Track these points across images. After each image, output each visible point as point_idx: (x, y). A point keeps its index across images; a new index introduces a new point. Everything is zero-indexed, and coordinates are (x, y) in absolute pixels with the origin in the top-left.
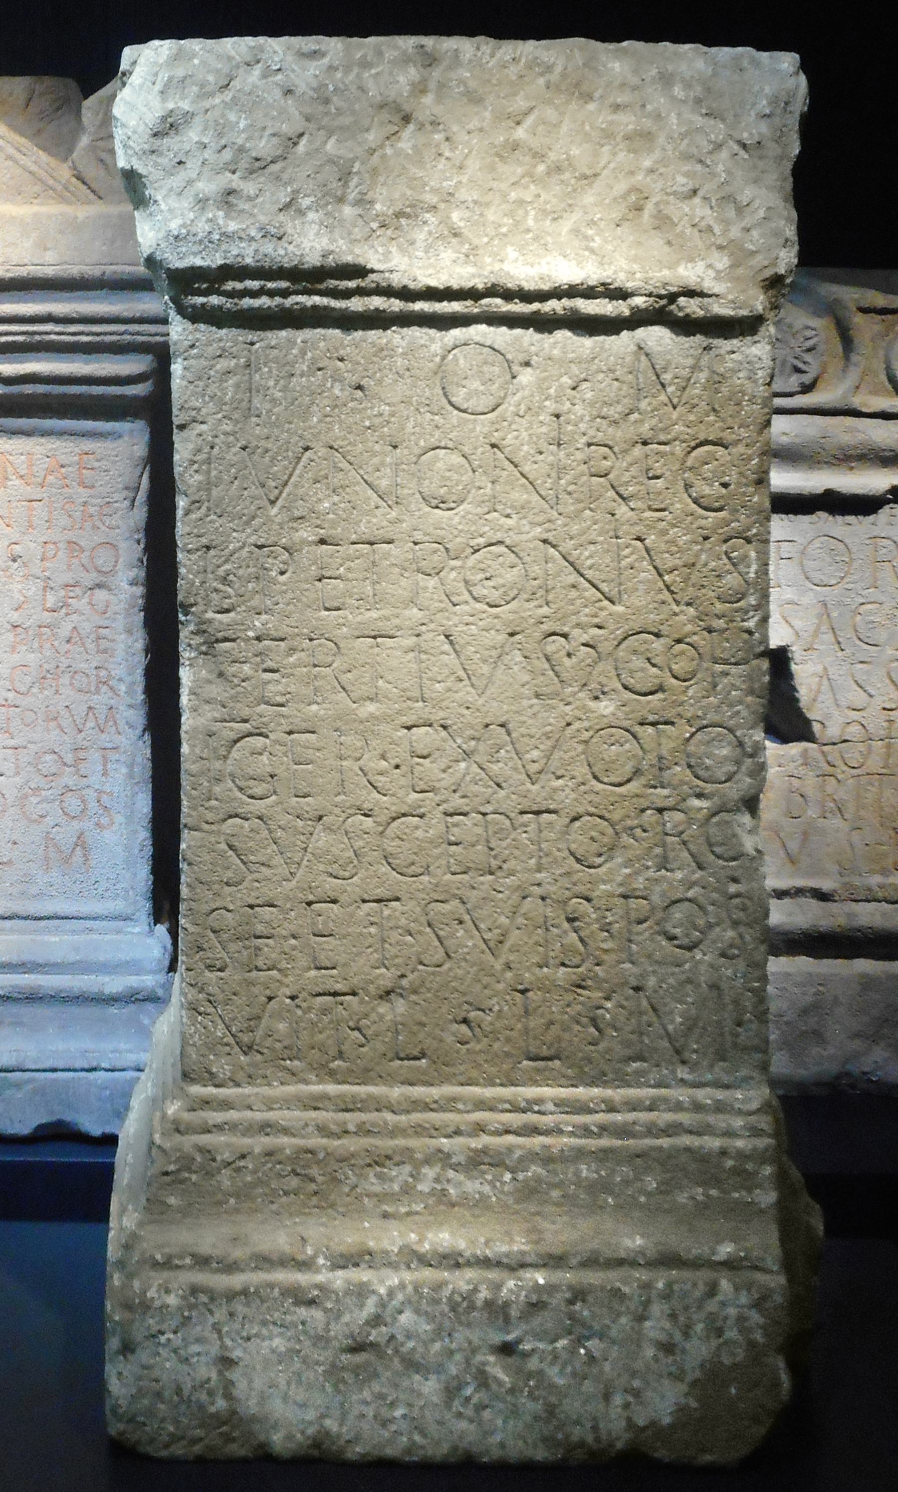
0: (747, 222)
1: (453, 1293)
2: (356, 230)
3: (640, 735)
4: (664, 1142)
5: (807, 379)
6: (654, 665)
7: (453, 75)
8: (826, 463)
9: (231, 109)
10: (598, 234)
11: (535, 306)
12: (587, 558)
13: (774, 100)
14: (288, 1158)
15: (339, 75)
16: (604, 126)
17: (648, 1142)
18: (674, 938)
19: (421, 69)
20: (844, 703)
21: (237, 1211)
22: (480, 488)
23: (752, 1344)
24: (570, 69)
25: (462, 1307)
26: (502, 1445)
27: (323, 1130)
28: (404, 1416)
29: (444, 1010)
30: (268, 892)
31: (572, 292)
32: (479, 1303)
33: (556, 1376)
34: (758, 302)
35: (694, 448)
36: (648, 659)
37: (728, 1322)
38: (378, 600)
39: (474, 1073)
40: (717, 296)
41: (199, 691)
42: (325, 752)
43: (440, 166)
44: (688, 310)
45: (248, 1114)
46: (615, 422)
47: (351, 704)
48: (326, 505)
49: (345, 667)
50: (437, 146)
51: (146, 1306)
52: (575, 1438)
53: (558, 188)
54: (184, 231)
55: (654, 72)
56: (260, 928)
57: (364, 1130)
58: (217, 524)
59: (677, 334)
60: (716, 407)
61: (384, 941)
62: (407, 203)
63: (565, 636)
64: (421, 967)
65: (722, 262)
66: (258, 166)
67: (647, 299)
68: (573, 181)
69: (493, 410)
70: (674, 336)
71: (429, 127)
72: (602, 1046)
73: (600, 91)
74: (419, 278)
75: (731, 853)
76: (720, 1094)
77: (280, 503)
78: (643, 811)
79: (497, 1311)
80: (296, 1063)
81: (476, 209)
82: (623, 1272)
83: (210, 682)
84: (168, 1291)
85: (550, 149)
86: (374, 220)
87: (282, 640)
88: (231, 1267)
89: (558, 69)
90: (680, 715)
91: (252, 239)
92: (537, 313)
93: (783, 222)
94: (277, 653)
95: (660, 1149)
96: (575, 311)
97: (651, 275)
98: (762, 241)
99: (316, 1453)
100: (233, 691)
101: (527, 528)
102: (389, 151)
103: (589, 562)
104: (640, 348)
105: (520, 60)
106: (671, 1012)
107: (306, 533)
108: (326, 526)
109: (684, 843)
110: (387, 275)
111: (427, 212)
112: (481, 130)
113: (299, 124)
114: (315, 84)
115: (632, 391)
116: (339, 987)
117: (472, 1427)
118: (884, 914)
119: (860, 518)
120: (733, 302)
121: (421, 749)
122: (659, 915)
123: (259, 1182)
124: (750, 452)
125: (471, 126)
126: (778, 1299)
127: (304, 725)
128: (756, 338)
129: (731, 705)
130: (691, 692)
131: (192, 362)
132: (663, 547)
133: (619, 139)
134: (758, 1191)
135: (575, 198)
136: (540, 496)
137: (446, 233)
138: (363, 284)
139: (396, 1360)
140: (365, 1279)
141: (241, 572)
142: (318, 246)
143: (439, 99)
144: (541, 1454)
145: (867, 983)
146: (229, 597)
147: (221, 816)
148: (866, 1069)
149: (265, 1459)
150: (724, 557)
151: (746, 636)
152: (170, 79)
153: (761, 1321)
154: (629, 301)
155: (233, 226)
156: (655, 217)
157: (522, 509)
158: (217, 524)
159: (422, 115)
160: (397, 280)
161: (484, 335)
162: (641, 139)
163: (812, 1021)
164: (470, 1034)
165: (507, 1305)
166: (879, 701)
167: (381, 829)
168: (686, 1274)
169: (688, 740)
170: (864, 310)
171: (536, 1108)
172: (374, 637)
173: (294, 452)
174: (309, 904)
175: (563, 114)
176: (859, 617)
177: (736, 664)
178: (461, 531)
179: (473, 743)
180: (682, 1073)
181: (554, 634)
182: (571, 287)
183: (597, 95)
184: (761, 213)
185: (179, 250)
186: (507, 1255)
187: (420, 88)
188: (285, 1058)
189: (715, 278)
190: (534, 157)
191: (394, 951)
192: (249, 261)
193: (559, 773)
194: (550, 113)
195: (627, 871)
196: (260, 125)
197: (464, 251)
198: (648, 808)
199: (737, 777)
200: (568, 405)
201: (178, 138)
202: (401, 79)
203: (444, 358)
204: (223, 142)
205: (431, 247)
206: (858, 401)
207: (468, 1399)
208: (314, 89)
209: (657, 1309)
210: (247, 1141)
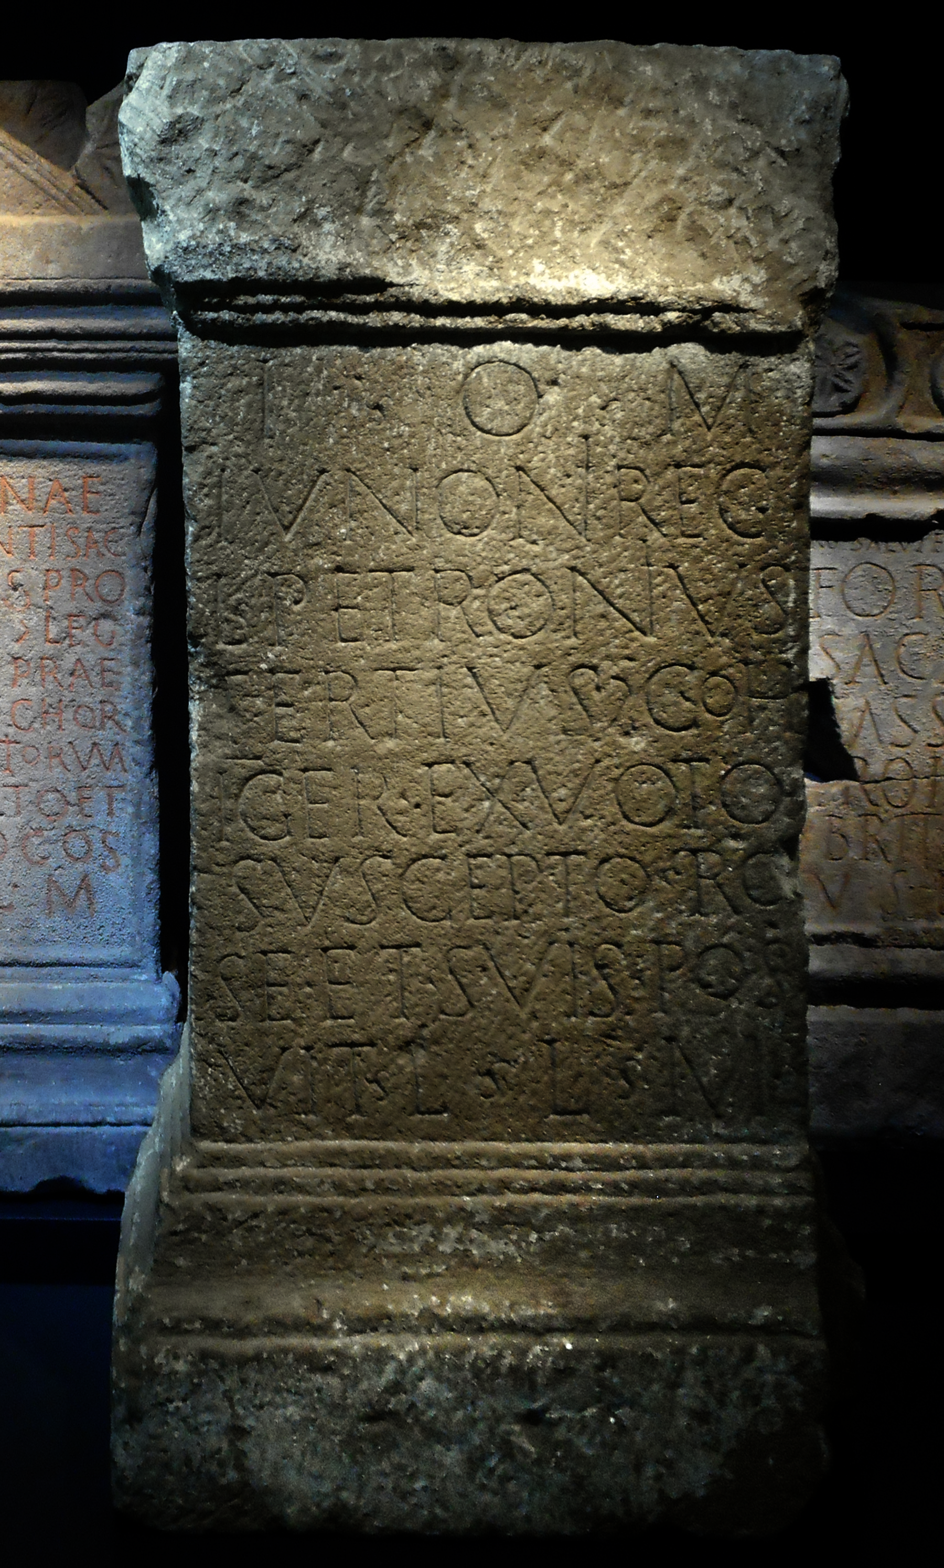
0: (785, 233)
1: (477, 1358)
2: (375, 241)
4: (698, 1200)
5: (848, 398)
6: (687, 699)
7: (476, 79)
8: (868, 486)
10: (628, 246)
11: (563, 322)
12: (617, 587)
13: (814, 106)
14: (303, 1217)
16: (635, 132)
20: (887, 739)
21: (249, 1272)
22: (504, 513)
24: (599, 73)
25: (486, 1373)
27: (339, 1187)
28: (425, 1488)
29: (467, 1061)
30: (281, 937)
32: (504, 1370)
38: (398, 631)
39: (499, 1128)
40: (754, 311)
42: (342, 790)
43: (463, 175)
44: (724, 326)
45: (261, 1171)
47: (369, 740)
48: (343, 531)
50: (460, 153)
53: (586, 197)
54: (193, 243)
55: (687, 75)
56: (273, 975)
57: (382, 1188)
58: (228, 551)
59: (712, 352)
63: (594, 668)
64: (442, 1017)
65: (759, 276)
66: (270, 175)
68: (602, 191)
69: (518, 431)
70: (708, 354)
71: (451, 134)
72: (633, 1099)
73: (631, 96)
74: (441, 292)
75: (769, 897)
76: (757, 1151)
77: (294, 528)
79: (523, 1378)
83: (220, 716)
84: (176, 1357)
85: (578, 156)
86: (393, 232)
87: (297, 672)
88: (244, 1332)
90: (715, 752)
91: (265, 251)
93: (822, 234)
96: (604, 327)
97: (684, 289)
98: (801, 253)
100: (245, 727)
101: (554, 555)
102: (409, 159)
104: (673, 366)
105: (546, 63)
106: (706, 1064)
107: (321, 561)
109: (719, 886)
110: (407, 288)
111: (449, 223)
112: (506, 136)
113: (314, 130)
114: (331, 88)
115: (664, 411)
117: (496, 1500)
118: (929, 961)
120: (770, 317)
121: (442, 786)
122: (693, 961)
123: (272, 1243)
124: (788, 475)
125: (495, 133)
130: (726, 728)
131: (202, 380)
132: (697, 574)
135: (604, 208)
136: (568, 521)
139: (417, 1430)
141: (253, 601)
142: (334, 259)
143: (462, 105)
145: (911, 1032)
146: (241, 628)
147: (232, 858)
150: (761, 585)
151: (784, 668)
152: (179, 83)
155: (244, 238)
157: (549, 535)
158: (228, 551)
161: (509, 352)
162: (674, 147)
164: (494, 1087)
166: (923, 737)
167: (400, 871)
169: (723, 777)
171: (564, 1165)
172: (394, 670)
173: (309, 475)
174: (325, 949)
175: (591, 120)
176: (903, 649)
178: (484, 558)
179: (497, 781)
180: (717, 1128)
181: (582, 666)
183: (627, 100)
184: (800, 224)
190: (561, 165)
191: (414, 999)
193: (588, 812)
194: (578, 119)
195: (659, 915)
196: (273, 131)
197: (487, 263)
200: (597, 425)
202: (422, 83)
203: (466, 376)
204: (235, 149)
205: (453, 260)
206: (901, 421)
208: (330, 94)
209: (689, 1376)
210: (260, 1199)
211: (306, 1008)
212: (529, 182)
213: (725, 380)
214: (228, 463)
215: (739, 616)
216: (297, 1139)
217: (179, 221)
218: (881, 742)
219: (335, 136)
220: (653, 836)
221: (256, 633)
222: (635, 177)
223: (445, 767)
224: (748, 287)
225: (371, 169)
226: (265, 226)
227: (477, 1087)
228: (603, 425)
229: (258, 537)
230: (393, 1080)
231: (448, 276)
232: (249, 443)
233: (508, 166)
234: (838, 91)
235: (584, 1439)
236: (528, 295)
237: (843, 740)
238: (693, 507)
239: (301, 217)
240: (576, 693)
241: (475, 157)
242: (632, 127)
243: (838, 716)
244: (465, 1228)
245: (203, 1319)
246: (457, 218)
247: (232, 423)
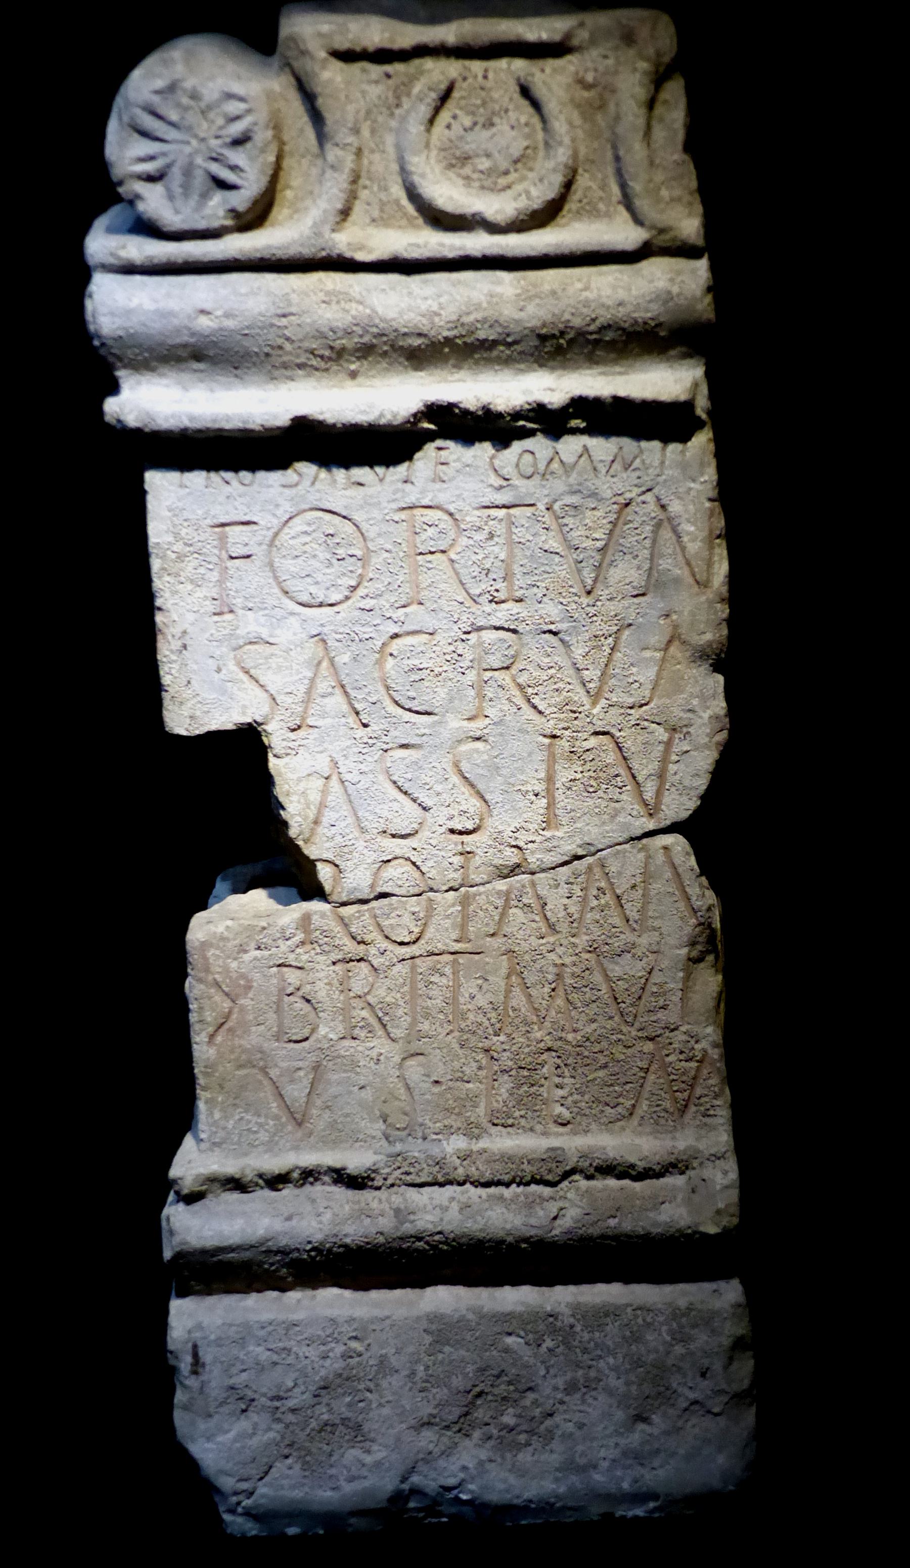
5: (241, 200)
8: (300, 366)
20: (373, 825)
118: (465, 1207)
119: (380, 470)
145: (442, 1331)
148: (451, 1482)
163: (341, 1406)
166: (440, 818)
170: (347, 56)
176: (390, 662)
206: (343, 241)
218: (363, 830)
237: (293, 832)
243: (280, 791)
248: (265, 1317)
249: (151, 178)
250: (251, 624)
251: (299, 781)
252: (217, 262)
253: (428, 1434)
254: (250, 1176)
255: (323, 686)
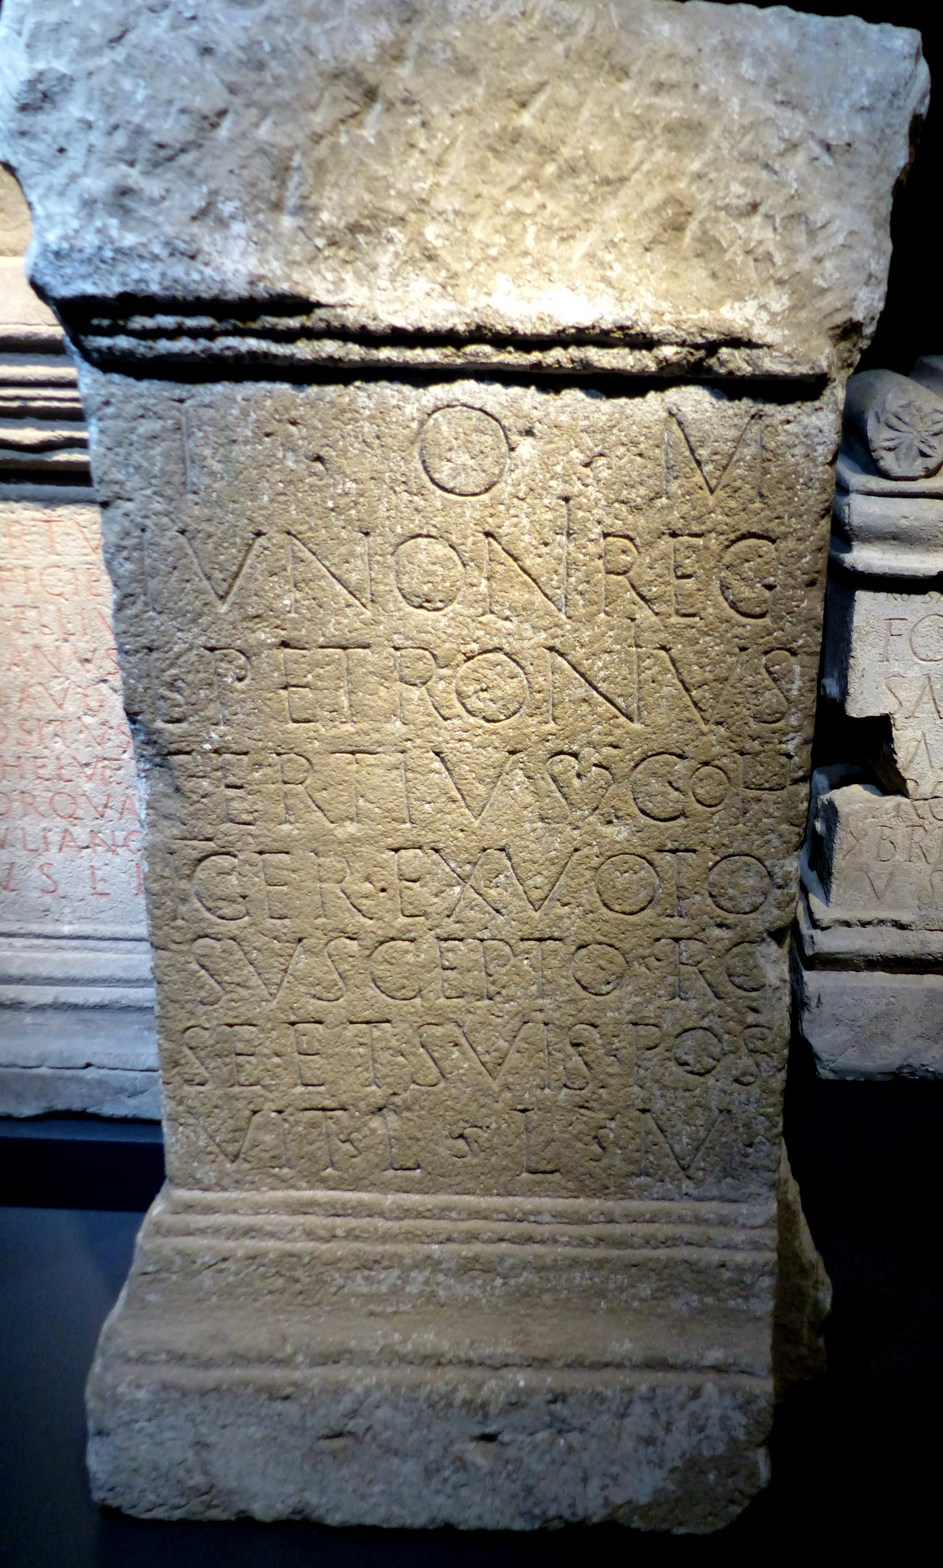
0: (818, 250)
1: (431, 1392)
2: (296, 248)
3: (656, 863)
4: (663, 1253)
6: (677, 789)
7: (438, 35)
9: (124, 73)
10: (618, 260)
11: (535, 356)
12: (601, 669)
13: (876, 90)
14: (272, 1261)
15: (280, 30)
16: (638, 112)
17: (647, 1253)
18: (687, 1064)
19: (397, 25)
21: (220, 1307)
22: (472, 585)
23: (733, 1440)
24: (599, 31)
25: (441, 1405)
26: (480, 1517)
27: (310, 1234)
28: (383, 1492)
29: (439, 1126)
30: (246, 1012)
31: (581, 337)
32: (457, 1402)
33: (533, 1463)
34: (823, 355)
35: (733, 542)
36: (670, 783)
37: (710, 1422)
38: (357, 712)
39: (470, 1185)
40: (769, 347)
41: (157, 805)
42: (302, 873)
43: (412, 162)
44: (731, 366)
45: (233, 1218)
46: (638, 508)
47: (328, 824)
48: (287, 602)
49: (320, 784)
50: (409, 133)
51: (116, 1401)
52: (552, 1512)
53: (571, 197)
54: (65, 245)
55: (715, 39)
56: (240, 1047)
57: (351, 1235)
58: (157, 623)
59: (719, 397)
60: (765, 492)
61: (375, 1061)
62: (366, 212)
63: (575, 755)
64: (413, 1086)
65: (779, 301)
66: (164, 156)
67: (679, 349)
68: (591, 187)
69: (487, 490)
70: (714, 401)
71: (400, 107)
72: (605, 1162)
73: (639, 63)
74: (382, 316)
75: (752, 984)
76: (726, 1209)
77: (231, 598)
78: (658, 940)
79: (477, 1409)
80: (286, 1170)
81: (458, 222)
82: (607, 1374)
83: (166, 795)
84: (139, 1387)
85: (563, 142)
86: (319, 235)
87: (246, 753)
88: (208, 1364)
89: (583, 30)
90: (703, 843)
91: (156, 258)
92: (538, 365)
93: (866, 253)
94: (240, 769)
95: (658, 1260)
96: (586, 364)
97: (684, 317)
98: (837, 275)
99: (298, 1517)
100: (192, 809)
101: (529, 633)
102: (343, 139)
103: (602, 674)
104: (671, 414)
105: (532, 16)
106: (679, 1134)
107: (265, 635)
108: (288, 626)
109: (701, 972)
110: (339, 311)
111: (394, 225)
112: (469, 112)
113: (220, 98)
114: (243, 40)
115: (659, 469)
116: (327, 1103)
117: (449, 1502)
120: (790, 355)
121: (409, 872)
122: (670, 1042)
123: (242, 1283)
124: (802, 547)
125: (457, 107)
126: (763, 1403)
127: (276, 846)
128: (817, 404)
129: (763, 834)
130: (716, 818)
131: (108, 423)
132: (692, 658)
133: (657, 131)
134: (754, 1300)
135: (591, 211)
136: (546, 595)
137: (418, 255)
138: (309, 324)
139: (374, 1446)
140: (342, 1377)
141: (190, 678)
142: (243, 270)
143: (419, 70)
144: (518, 1525)
146: (179, 706)
147: (189, 936)
149: (246, 1525)
150: (763, 671)
151: (783, 760)
152: (39, 25)
153: (744, 1421)
154: (656, 351)
155: (130, 240)
156: (699, 240)
157: (522, 611)
158: (157, 623)
159: (388, 91)
160: (352, 318)
161: (472, 394)
162: (686, 133)
163: (882, 1026)
164: (466, 1148)
165: (484, 1405)
167: (367, 952)
168: (671, 1376)
169: (711, 869)
171: (532, 1218)
172: (353, 753)
173: (243, 538)
174: (293, 1024)
175: (584, 93)
177: (770, 789)
178: (450, 635)
179: (468, 867)
180: (687, 1186)
181: (561, 753)
182: (580, 330)
183: (634, 69)
184: (841, 239)
185: (63, 271)
186: (490, 1357)
187: (393, 54)
188: (269, 1166)
189: (772, 324)
190: (540, 153)
191: (385, 1071)
192: (155, 288)
193: (565, 900)
194: (567, 92)
195: (638, 999)
196: (164, 96)
197: (440, 280)
198: (663, 937)
199: (762, 909)
200: (579, 486)
201: (56, 115)
202: (366, 37)
203: (422, 423)
204: (113, 120)
205: (397, 274)
207: (446, 1480)
208: (242, 48)
209: (638, 1408)
210: (231, 1244)
211: (274, 1076)
212: (498, 174)
213: (734, 433)
214: (148, 522)
215: (738, 704)
216: (272, 1189)
217: (49, 217)
219: (248, 106)
220: (634, 925)
221: (196, 712)
222: (635, 170)
223: (411, 852)
224: (765, 316)
225: (291, 151)
226: (156, 225)
227: (450, 1149)
228: (587, 486)
229: (189, 608)
230: (366, 1141)
231: (391, 294)
232: (171, 500)
233: (471, 153)
234: (913, 76)
235: (535, 1457)
236: (489, 322)
238: (689, 584)
239: (200, 216)
240: (555, 780)
241: (428, 139)
242: (636, 105)
243: (896, 745)
244: (433, 1272)
245: (169, 1352)
246: (402, 219)
247: (149, 476)
248: (854, 984)
249: (890, 449)
250: (896, 668)
251: (906, 742)
252: (43, 357)
253: (919, 1041)
254: (854, 921)
255: (925, 699)
